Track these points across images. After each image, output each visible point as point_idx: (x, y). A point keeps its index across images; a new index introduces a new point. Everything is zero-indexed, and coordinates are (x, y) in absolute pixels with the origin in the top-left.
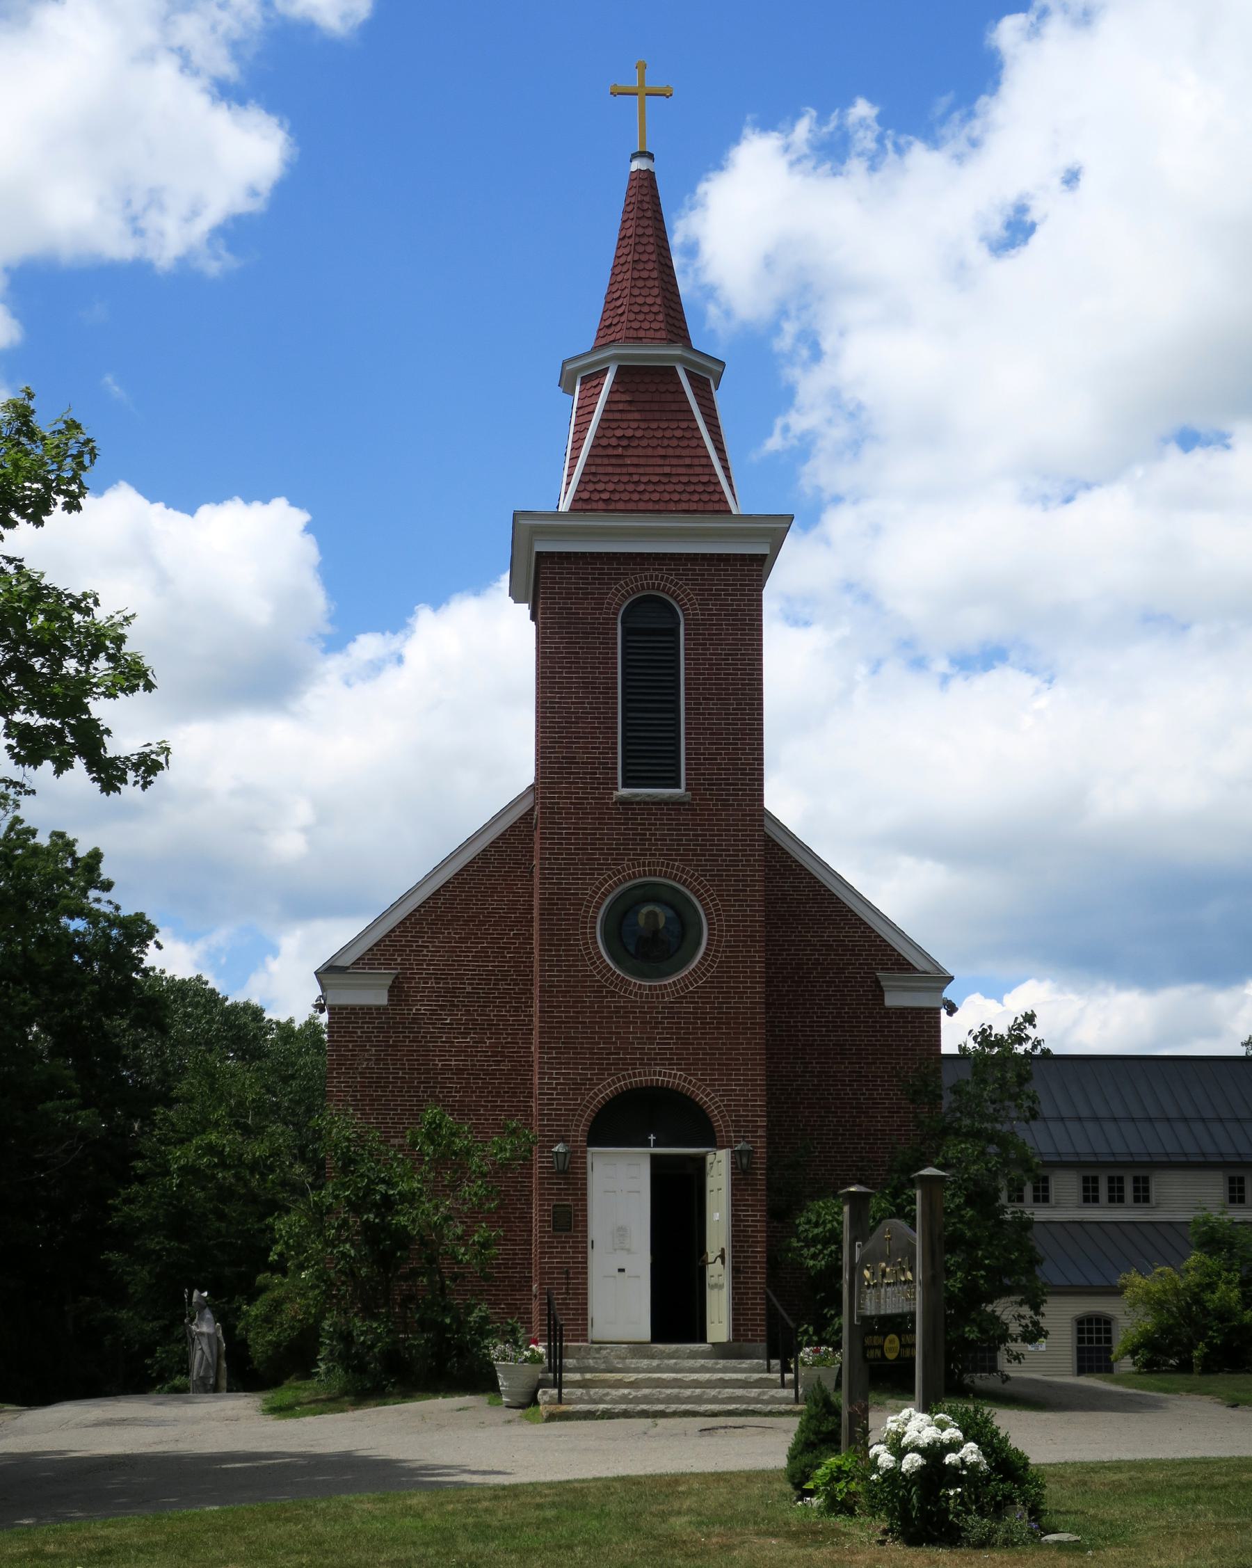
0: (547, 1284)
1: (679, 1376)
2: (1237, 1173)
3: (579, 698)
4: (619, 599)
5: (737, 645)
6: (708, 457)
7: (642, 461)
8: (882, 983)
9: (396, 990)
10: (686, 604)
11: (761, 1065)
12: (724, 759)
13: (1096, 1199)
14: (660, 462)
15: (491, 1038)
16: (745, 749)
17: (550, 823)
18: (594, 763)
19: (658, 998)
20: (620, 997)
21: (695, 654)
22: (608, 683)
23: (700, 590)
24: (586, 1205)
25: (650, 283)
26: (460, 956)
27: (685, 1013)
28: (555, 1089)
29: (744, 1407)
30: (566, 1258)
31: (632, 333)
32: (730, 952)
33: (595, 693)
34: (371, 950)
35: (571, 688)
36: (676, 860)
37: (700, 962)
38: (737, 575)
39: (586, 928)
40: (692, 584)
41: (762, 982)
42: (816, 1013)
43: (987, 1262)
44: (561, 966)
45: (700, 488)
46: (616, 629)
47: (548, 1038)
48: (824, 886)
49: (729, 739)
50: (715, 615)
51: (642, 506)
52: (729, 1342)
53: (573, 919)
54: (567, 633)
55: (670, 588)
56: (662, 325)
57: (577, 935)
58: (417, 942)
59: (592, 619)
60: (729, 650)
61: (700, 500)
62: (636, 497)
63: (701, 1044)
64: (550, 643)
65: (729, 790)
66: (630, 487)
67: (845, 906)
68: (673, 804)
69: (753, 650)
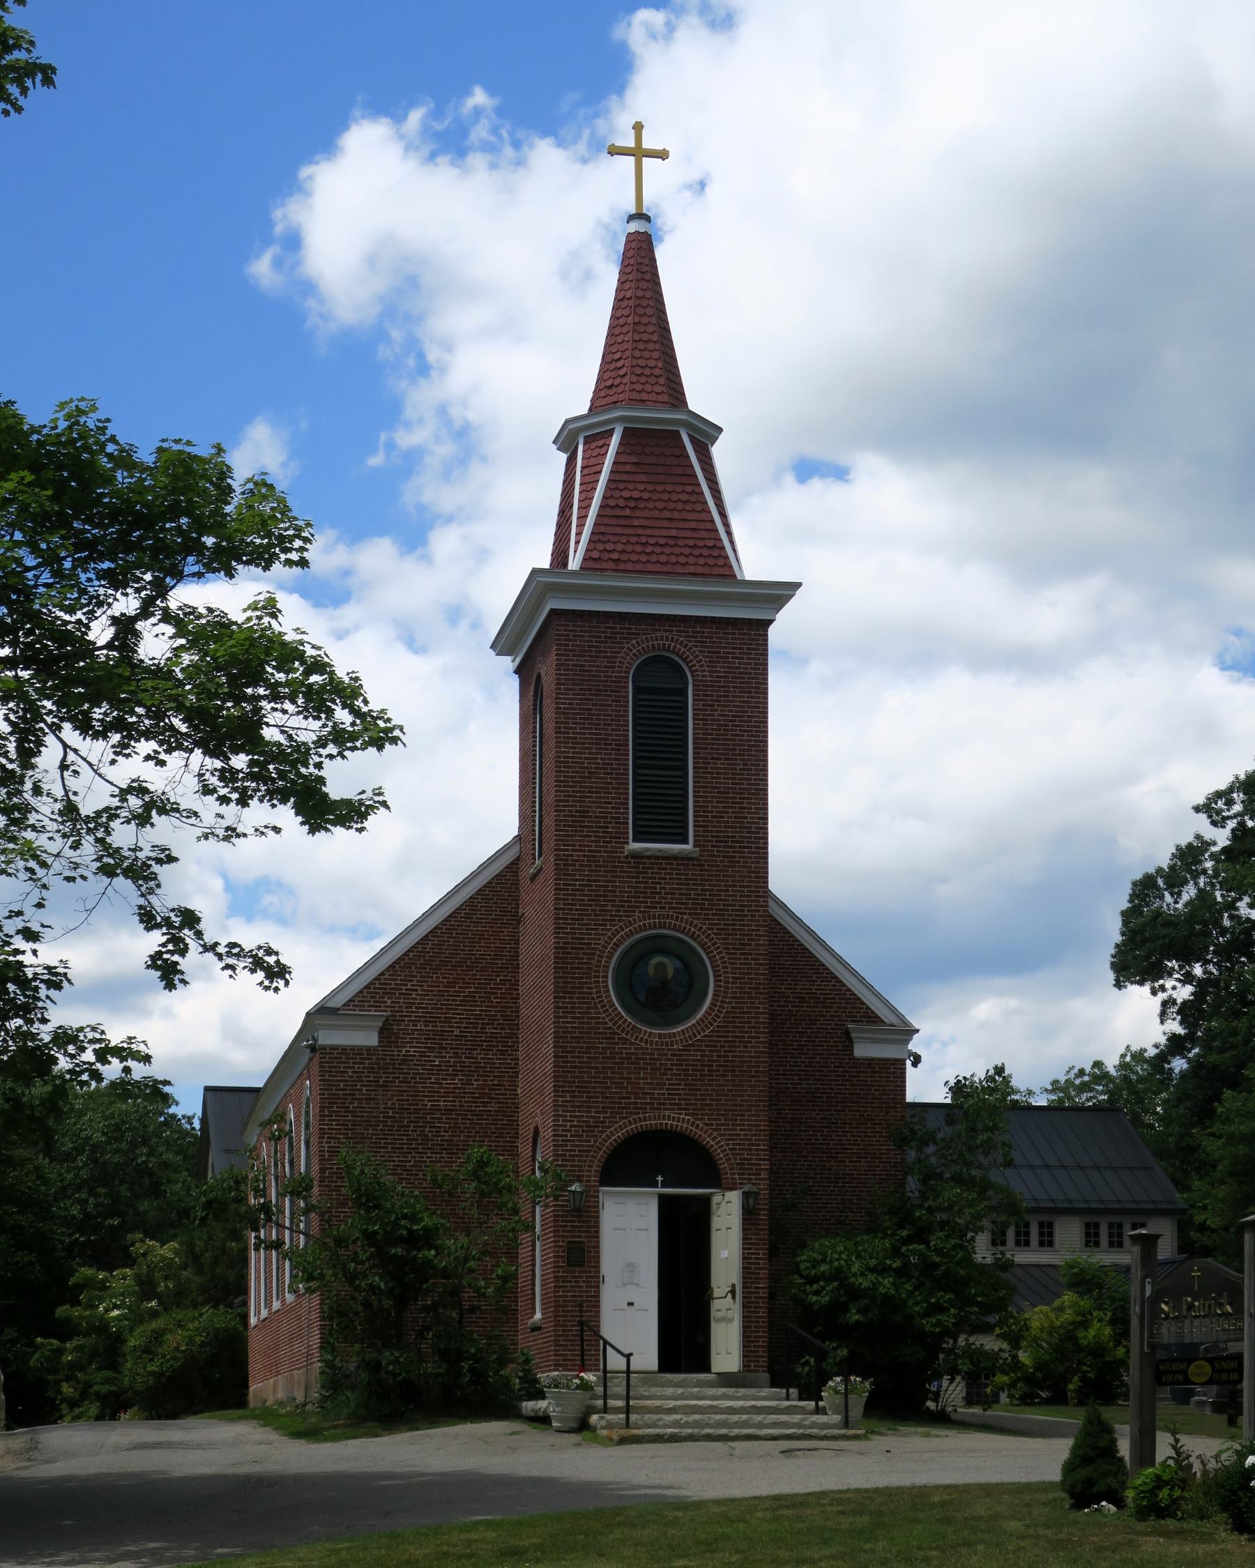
0: (561, 1316)
1: (715, 1403)
2: (1092, 1219)
3: (593, 753)
4: (630, 658)
5: (743, 707)
6: (713, 522)
7: (650, 523)
8: (853, 1035)
9: (385, 1032)
10: (695, 665)
11: (764, 1111)
12: (731, 817)
13: (1027, 1243)
14: (666, 524)
15: (478, 1080)
16: (751, 808)
17: (564, 874)
18: (607, 818)
19: (667, 1045)
20: (631, 1044)
21: (703, 715)
22: (619, 740)
23: (708, 652)
24: (598, 1242)
25: (651, 346)
26: (448, 1000)
27: (693, 1060)
28: (569, 1131)
29: (801, 1431)
30: (579, 1292)
31: (635, 395)
32: (736, 1003)
33: (607, 749)
34: (361, 992)
35: (585, 743)
36: (684, 914)
37: (706, 1012)
38: (743, 639)
39: (598, 977)
40: (701, 647)
41: (766, 1033)
42: (789, 1062)
43: (979, 1299)
44: (574, 1013)
45: (706, 552)
46: (628, 688)
47: (563, 1082)
48: (798, 941)
49: (736, 798)
50: (722, 677)
51: (650, 567)
52: (739, 1372)
53: (587, 968)
54: (580, 689)
55: (680, 649)
56: (664, 389)
57: (591, 983)
58: (407, 985)
59: (604, 676)
60: (736, 711)
61: (706, 563)
62: (644, 558)
63: (707, 1090)
64: (564, 699)
65: (735, 847)
66: (639, 548)
67: (817, 960)
68: (682, 859)
69: (759, 712)
